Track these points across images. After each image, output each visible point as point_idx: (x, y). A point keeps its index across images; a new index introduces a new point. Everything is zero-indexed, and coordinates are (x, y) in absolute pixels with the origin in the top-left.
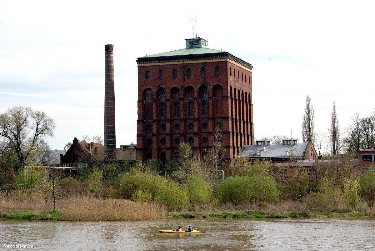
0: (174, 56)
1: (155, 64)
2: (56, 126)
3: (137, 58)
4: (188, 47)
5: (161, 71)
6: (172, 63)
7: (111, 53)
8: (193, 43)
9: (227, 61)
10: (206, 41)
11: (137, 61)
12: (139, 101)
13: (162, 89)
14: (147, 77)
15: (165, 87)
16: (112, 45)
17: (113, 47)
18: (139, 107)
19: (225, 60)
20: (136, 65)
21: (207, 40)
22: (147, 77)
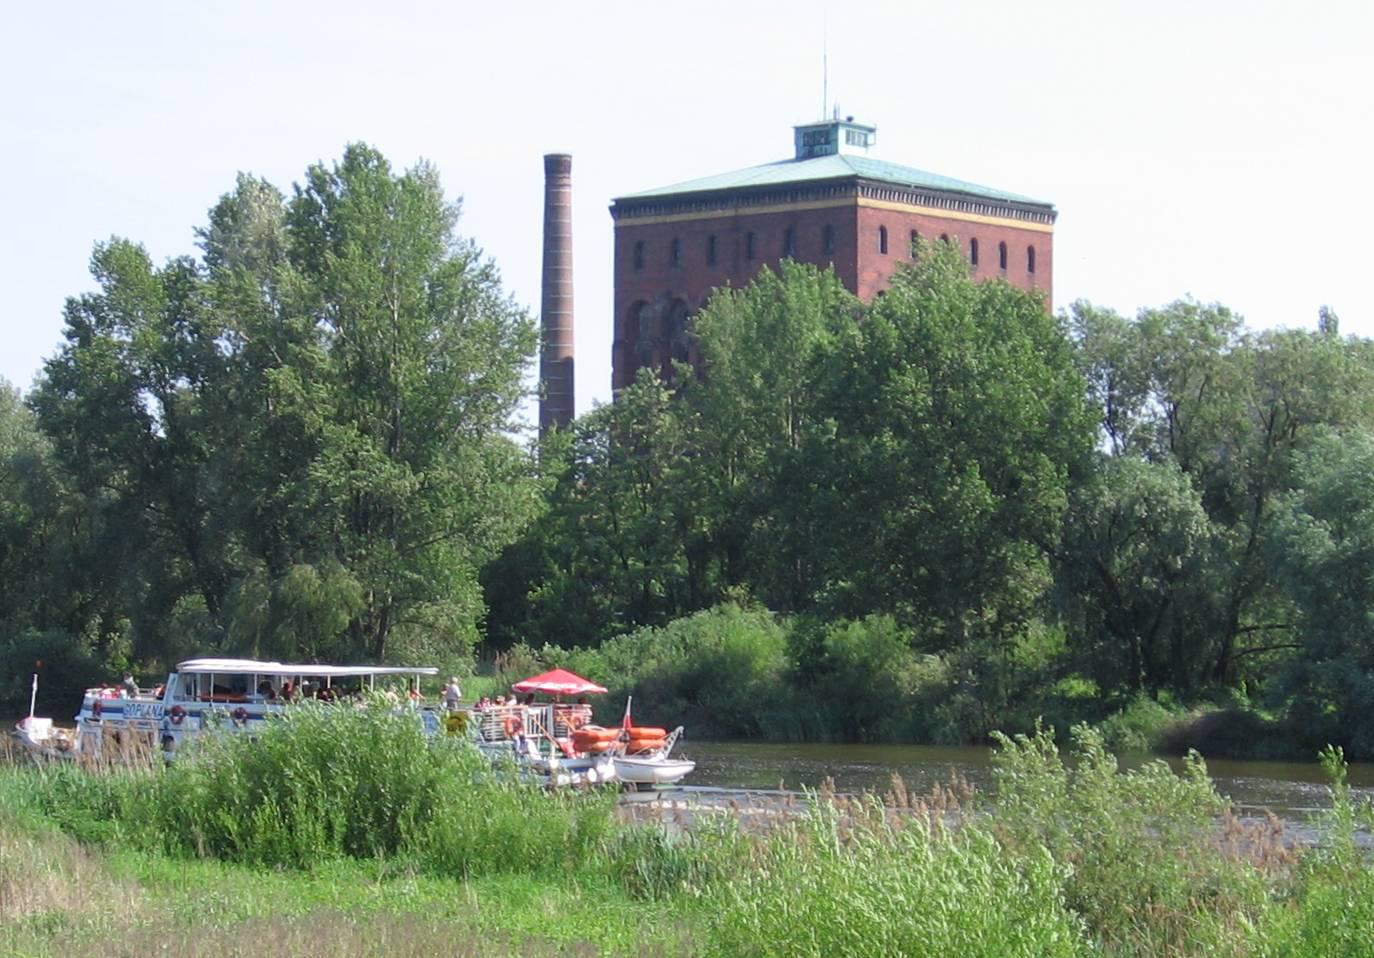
0: (945, 185)
1: (660, 219)
2: (485, 275)
3: (263, 179)
4: (801, 155)
5: (675, 242)
6: (705, 214)
7: (566, 181)
8: (815, 140)
9: (855, 208)
10: (872, 130)
11: (312, 169)
12: (617, 346)
13: (679, 301)
14: (639, 263)
15: (684, 296)
16: (565, 156)
17: (570, 163)
18: (614, 363)
19: (849, 202)
20: (608, 224)
21: (871, 125)
22: (639, 263)
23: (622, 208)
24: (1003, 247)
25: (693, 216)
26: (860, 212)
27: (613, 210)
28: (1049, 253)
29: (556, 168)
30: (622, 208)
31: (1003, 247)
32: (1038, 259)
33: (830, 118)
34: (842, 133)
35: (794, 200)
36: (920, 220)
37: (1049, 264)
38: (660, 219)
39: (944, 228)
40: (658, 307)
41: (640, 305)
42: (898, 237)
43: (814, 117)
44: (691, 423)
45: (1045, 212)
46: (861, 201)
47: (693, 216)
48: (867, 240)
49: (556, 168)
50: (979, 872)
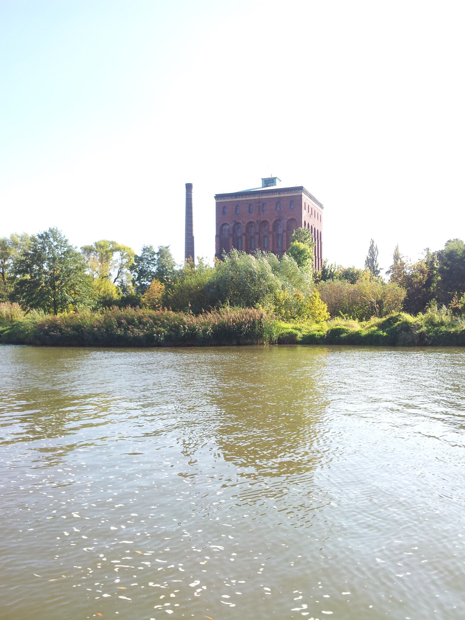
1: (232, 200)
8: (268, 181)
22: (224, 213)
35: (236, 198)
46: (303, 194)
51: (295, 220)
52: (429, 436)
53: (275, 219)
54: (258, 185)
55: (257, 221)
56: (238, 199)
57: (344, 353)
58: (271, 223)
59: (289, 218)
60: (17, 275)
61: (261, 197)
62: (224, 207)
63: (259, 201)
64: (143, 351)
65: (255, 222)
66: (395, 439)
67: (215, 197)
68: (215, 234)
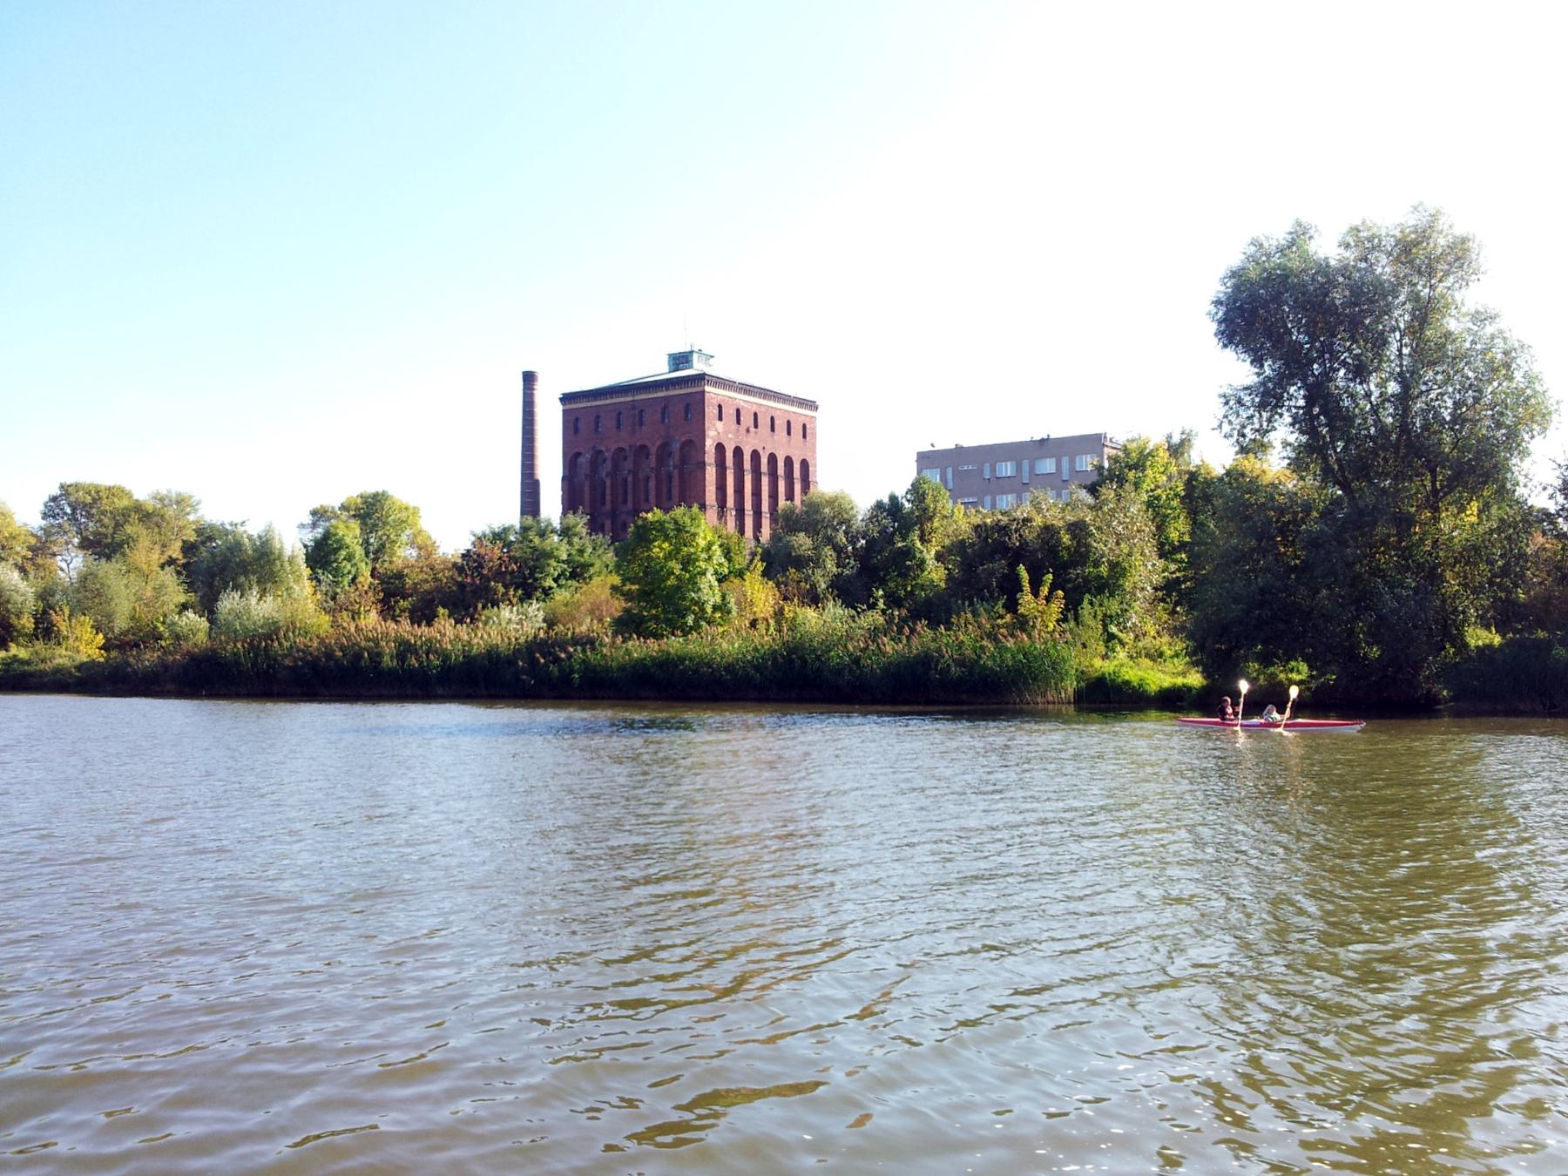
1: (589, 404)
5: (598, 417)
8: (680, 360)
12: (564, 479)
14: (576, 430)
22: (576, 430)
23: (567, 398)
24: (789, 423)
25: (608, 402)
26: (707, 395)
27: (561, 399)
28: (814, 429)
29: (529, 378)
30: (567, 398)
31: (789, 423)
32: (808, 431)
33: (688, 349)
34: (695, 356)
35: (667, 389)
36: (742, 403)
37: (814, 435)
38: (589, 404)
39: (755, 408)
40: (588, 456)
41: (578, 455)
42: (729, 412)
43: (684, 348)
44: (668, 612)
45: (811, 405)
46: (707, 388)
47: (608, 402)
48: (711, 412)
49: (529, 378)
50: (1276, 755)
51: (691, 441)
52: (947, 954)
53: (659, 443)
54: (658, 369)
55: (631, 446)
56: (598, 403)
57: (1094, 728)
58: (653, 450)
59: (683, 439)
60: (84, 579)
61: (637, 398)
62: (577, 419)
63: (633, 405)
64: (870, 713)
65: (627, 448)
66: (880, 964)
67: (1459, 255)
68: (561, 475)
